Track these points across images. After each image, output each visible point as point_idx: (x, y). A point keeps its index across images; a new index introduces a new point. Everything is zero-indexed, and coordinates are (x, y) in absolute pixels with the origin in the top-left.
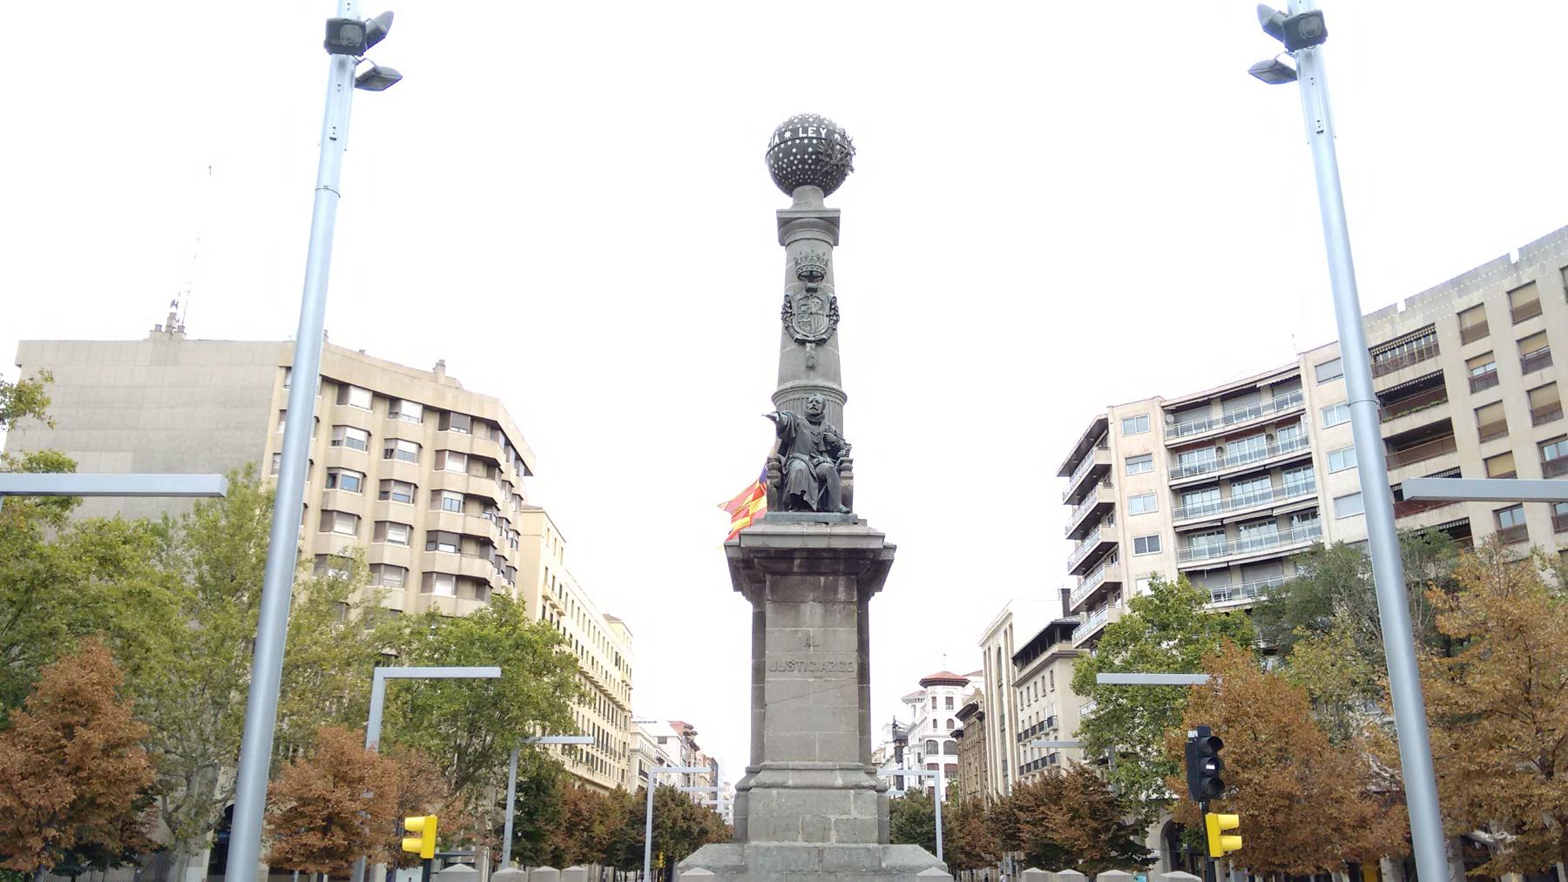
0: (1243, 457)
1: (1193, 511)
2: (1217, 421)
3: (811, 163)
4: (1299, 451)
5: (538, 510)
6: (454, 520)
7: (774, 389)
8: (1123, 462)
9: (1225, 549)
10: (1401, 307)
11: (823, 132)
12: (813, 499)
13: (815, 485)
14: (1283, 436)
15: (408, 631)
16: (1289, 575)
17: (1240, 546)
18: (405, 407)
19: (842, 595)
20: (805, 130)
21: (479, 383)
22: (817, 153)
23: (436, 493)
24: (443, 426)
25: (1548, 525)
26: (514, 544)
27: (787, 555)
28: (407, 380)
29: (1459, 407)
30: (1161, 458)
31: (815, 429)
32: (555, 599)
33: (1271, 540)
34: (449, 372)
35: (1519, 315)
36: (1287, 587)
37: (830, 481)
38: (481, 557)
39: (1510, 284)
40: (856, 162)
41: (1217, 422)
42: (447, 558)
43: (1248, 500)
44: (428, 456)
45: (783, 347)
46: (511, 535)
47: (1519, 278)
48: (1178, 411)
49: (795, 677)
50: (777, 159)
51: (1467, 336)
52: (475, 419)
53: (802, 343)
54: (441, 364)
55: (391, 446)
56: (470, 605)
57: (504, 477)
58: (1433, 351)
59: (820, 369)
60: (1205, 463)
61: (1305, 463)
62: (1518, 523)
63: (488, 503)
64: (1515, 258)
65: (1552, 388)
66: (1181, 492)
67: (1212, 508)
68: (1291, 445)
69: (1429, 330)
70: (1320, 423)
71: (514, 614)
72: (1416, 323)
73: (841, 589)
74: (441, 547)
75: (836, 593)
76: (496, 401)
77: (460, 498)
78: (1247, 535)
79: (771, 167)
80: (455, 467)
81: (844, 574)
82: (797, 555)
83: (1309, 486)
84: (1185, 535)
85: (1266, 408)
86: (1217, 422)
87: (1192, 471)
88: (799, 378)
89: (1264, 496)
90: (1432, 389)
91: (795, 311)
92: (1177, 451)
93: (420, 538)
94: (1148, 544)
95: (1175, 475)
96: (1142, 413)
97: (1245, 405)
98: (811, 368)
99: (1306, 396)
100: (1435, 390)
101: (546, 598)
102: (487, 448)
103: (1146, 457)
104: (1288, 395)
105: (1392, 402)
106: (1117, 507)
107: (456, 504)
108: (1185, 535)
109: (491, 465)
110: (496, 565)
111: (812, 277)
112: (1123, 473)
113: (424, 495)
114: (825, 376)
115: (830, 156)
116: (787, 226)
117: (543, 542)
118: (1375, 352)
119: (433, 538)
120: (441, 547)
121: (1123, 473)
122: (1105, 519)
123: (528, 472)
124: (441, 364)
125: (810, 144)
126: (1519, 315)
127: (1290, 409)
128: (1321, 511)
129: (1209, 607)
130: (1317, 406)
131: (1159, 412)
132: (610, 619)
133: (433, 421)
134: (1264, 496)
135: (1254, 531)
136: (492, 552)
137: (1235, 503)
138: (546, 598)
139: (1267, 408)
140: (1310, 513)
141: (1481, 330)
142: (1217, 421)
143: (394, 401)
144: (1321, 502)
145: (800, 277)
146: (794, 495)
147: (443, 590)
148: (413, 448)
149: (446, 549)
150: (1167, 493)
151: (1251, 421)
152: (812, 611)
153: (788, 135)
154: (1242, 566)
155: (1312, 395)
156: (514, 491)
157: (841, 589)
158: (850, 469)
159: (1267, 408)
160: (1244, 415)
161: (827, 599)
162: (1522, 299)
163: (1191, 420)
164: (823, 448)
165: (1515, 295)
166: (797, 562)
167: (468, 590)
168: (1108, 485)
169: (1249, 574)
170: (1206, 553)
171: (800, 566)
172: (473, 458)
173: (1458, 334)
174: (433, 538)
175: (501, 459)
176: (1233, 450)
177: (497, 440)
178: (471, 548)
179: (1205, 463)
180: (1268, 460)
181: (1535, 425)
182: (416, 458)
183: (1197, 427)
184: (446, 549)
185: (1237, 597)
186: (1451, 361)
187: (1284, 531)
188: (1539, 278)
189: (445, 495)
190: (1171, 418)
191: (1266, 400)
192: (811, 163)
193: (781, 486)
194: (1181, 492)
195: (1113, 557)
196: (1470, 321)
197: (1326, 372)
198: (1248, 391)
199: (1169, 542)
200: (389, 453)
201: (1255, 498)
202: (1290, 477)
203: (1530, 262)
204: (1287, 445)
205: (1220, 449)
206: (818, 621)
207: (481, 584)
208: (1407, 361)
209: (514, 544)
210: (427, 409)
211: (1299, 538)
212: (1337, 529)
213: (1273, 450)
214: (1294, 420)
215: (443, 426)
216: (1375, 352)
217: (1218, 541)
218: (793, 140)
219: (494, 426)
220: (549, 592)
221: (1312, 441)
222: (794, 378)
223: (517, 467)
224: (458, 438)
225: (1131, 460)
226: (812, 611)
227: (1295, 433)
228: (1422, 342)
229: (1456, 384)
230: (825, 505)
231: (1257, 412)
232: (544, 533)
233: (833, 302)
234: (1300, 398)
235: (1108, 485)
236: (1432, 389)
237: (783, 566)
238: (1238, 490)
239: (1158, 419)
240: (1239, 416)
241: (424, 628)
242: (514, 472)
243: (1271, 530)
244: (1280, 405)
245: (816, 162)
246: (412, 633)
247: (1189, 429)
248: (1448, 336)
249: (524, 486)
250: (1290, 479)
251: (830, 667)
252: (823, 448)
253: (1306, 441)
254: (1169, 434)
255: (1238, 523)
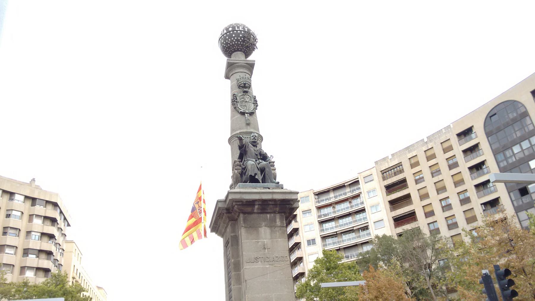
0: (342, 210)
1: (326, 229)
2: (332, 197)
3: (238, 44)
4: (361, 207)
5: (72, 242)
6: (35, 243)
7: (229, 136)
8: (301, 213)
9: (338, 242)
10: (390, 157)
11: (246, 29)
12: (259, 177)
13: (259, 173)
14: (354, 202)
15: (14, 290)
16: (367, 248)
17: (343, 241)
18: (17, 197)
19: (278, 223)
20: (238, 27)
21: (48, 188)
22: (244, 37)
23: (29, 233)
24: (33, 205)
25: (446, 227)
26: (62, 254)
27: (251, 203)
28: (18, 185)
29: (412, 189)
30: (314, 211)
31: (255, 148)
32: (77, 278)
33: (353, 238)
34: (37, 183)
35: (429, 158)
36: (368, 252)
37: (267, 169)
38: (47, 259)
39: (425, 149)
40: (258, 45)
41: (332, 198)
42: (32, 260)
43: (345, 224)
44: (26, 217)
45: (232, 117)
46: (61, 251)
47: (428, 146)
48: (319, 194)
49: (259, 265)
50: (225, 40)
51: (413, 166)
52: (47, 202)
53: (243, 114)
54: (34, 180)
55: (9, 213)
56: (41, 280)
57: (59, 226)
58: (402, 171)
59: (251, 125)
60: (329, 212)
61: (363, 210)
62: (436, 227)
63: (51, 237)
64: (426, 140)
65: (442, 182)
66: (322, 223)
67: (333, 228)
68: (357, 204)
69: (400, 164)
70: (367, 197)
71: (62, 281)
72: (396, 162)
73: (278, 220)
74: (30, 256)
75: (275, 222)
76: (57, 195)
77: (39, 234)
78: (345, 237)
79: (222, 44)
80: (38, 222)
81: (279, 213)
82: (257, 203)
83: (365, 218)
84: (324, 238)
85: (348, 192)
86: (332, 198)
87: (325, 215)
88: (243, 129)
89: (350, 223)
90: (403, 183)
91: (238, 100)
92: (319, 208)
93: (20, 252)
94: (311, 242)
95: (319, 217)
96: (307, 195)
97: (341, 192)
98: (248, 124)
99: (361, 188)
100: (403, 184)
101: (74, 278)
102: (52, 212)
103: (309, 211)
104: (355, 188)
105: (390, 189)
106: (300, 229)
107: (37, 237)
108: (324, 238)
109: (53, 221)
110: (54, 263)
111: (245, 86)
112: (301, 217)
113: (23, 234)
114: (254, 128)
115: (249, 39)
116: (231, 68)
117: (73, 254)
118: (383, 172)
119: (26, 252)
120: (30, 256)
121: (301, 217)
122: (295, 234)
123: (69, 225)
124: (34, 180)
125: (241, 33)
126: (429, 158)
127: (357, 192)
128: (370, 227)
129: (344, 261)
130: (366, 191)
131: (313, 195)
132: (99, 288)
133: (29, 203)
134: (350, 223)
135: (347, 235)
136: (52, 258)
137: (341, 226)
138: (74, 278)
139: (348, 193)
140: (366, 228)
141: (417, 164)
142: (332, 197)
143: (12, 194)
144: (369, 224)
145: (239, 87)
146: (251, 176)
147: (30, 274)
148: (19, 214)
149: (32, 257)
150: (317, 224)
151: (343, 197)
152: (264, 231)
153: (230, 29)
154: (344, 248)
155: (363, 187)
156: (63, 232)
157: (278, 220)
158: (273, 166)
159: (348, 193)
160: (341, 195)
161: (271, 225)
162: (429, 153)
163: (324, 197)
164: (259, 157)
165: (427, 152)
166: (256, 207)
167: (41, 274)
168: (296, 221)
169: (347, 250)
170: (332, 245)
171: (258, 209)
172: (46, 218)
173: (409, 165)
174: (26, 252)
175: (58, 218)
176: (338, 207)
177: (57, 210)
178: (43, 256)
179: (329, 212)
180: (350, 210)
181: (456, 187)
182: (21, 218)
183: (326, 200)
184: (32, 257)
185: (352, 257)
186: (408, 174)
187: (358, 235)
188: (434, 146)
189: (33, 233)
190: (316, 197)
191: (348, 190)
192: (238, 44)
193: (242, 174)
194: (322, 223)
195: (299, 248)
196: (413, 161)
197: (367, 179)
198: (341, 187)
199: (319, 240)
200: (8, 216)
201: (347, 224)
202: (358, 216)
203: (431, 141)
204: (356, 205)
205: (334, 207)
206: (268, 236)
207: (47, 271)
208: (393, 175)
209: (62, 254)
210: (26, 197)
211: (363, 237)
212: (375, 232)
213: (352, 207)
214: (357, 196)
215: (33, 205)
216: (383, 172)
217: (335, 240)
218: (233, 31)
219: (55, 205)
220: (75, 275)
221: (365, 203)
222: (240, 129)
223: (64, 222)
224: (39, 209)
225: (304, 212)
226: (264, 231)
227: (358, 201)
228: (398, 168)
229: (410, 182)
230: (264, 181)
231: (345, 194)
232: (74, 251)
233: (255, 98)
234: (359, 188)
235: (296, 221)
236: (403, 183)
237: (249, 209)
238: (341, 221)
239: (312, 197)
240: (339, 195)
241: (21, 289)
242: (63, 224)
243: (353, 235)
244: (353, 191)
245: (243, 41)
246: (16, 291)
247: (323, 201)
248: (406, 166)
249: (67, 230)
250: (358, 217)
251: (276, 259)
252: (259, 157)
253: (362, 203)
254: (316, 202)
255: (341, 233)
